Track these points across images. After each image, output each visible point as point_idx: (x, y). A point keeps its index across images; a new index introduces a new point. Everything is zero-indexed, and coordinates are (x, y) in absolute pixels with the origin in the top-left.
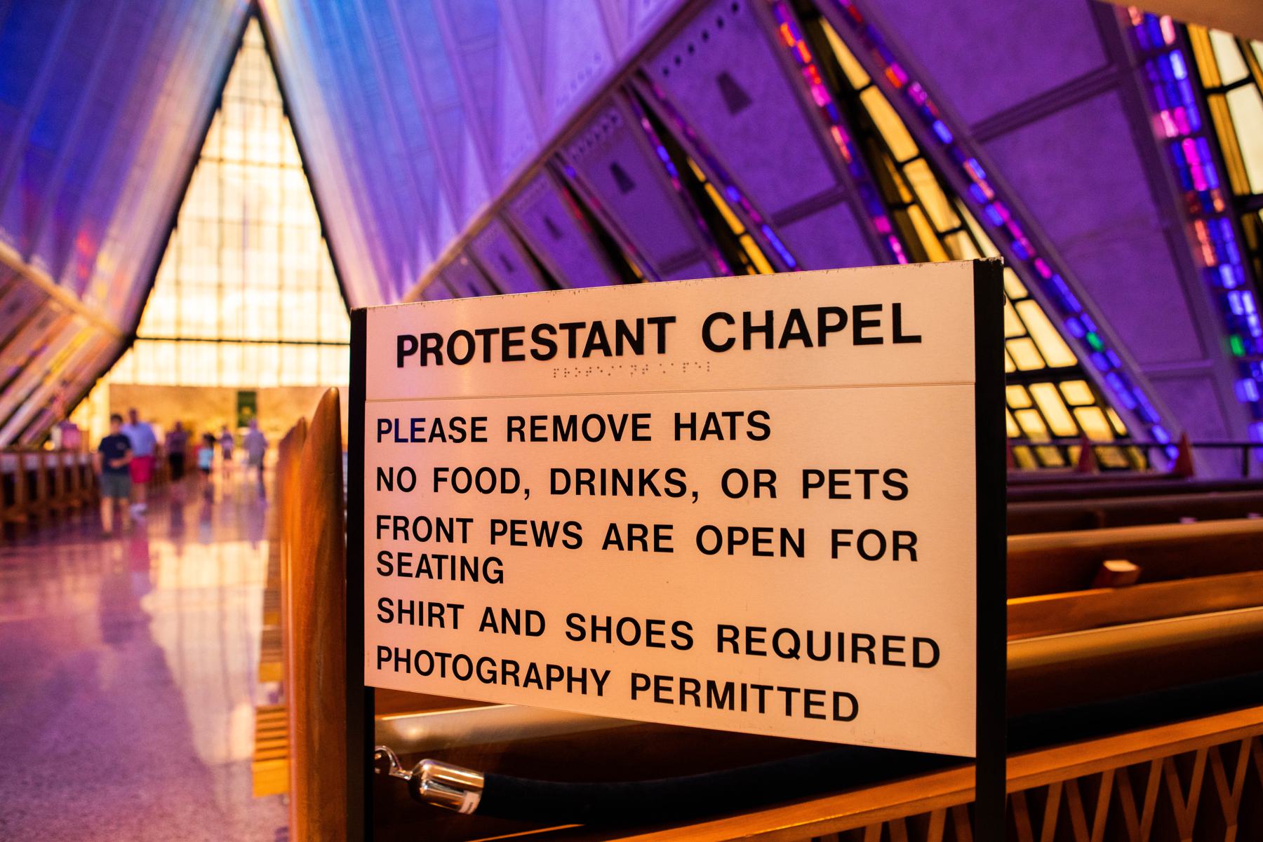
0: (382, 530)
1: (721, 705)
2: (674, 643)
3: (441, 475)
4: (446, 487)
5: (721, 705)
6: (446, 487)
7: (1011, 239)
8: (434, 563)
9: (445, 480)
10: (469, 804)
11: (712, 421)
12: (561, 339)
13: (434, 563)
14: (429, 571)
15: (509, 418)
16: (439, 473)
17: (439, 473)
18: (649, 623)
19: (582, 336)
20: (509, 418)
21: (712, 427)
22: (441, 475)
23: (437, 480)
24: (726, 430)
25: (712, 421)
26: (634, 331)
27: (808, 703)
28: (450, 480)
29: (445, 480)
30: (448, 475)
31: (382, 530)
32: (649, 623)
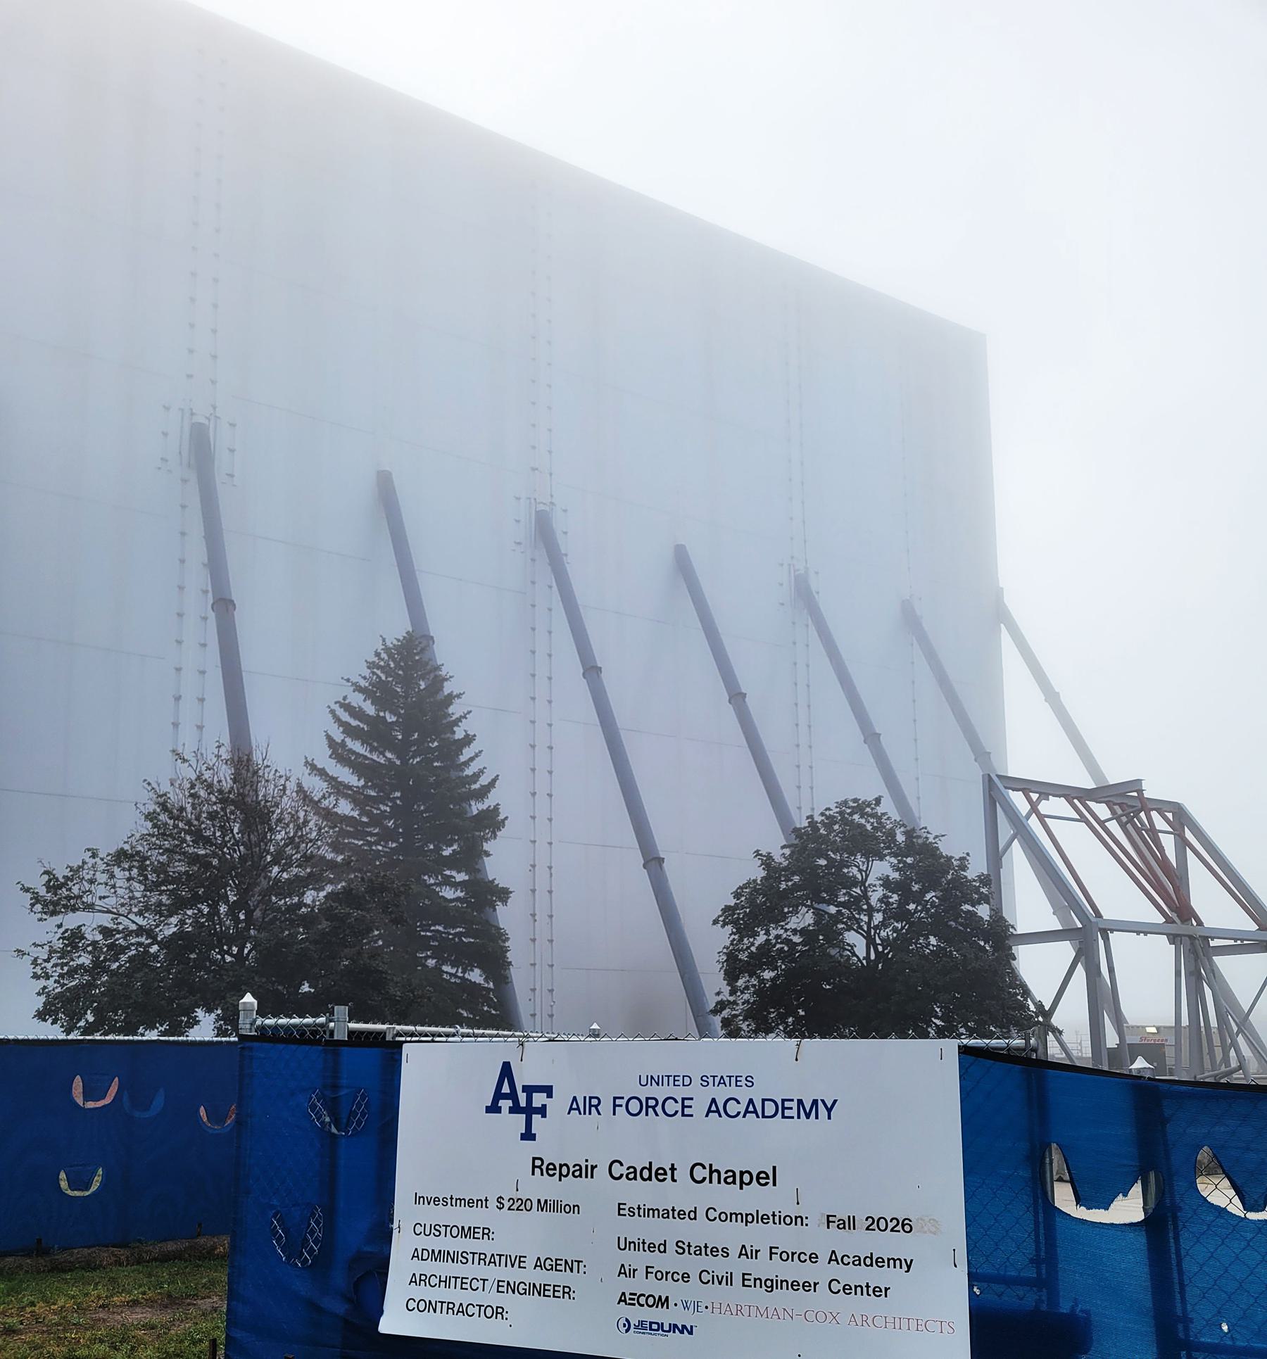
0: (617, 1108)
1: (808, 1116)
2: (746, 1085)
3: (618, 1102)
4: (621, 1111)
5: (808, 1116)
6: (621, 1111)
7: (74, 989)
8: (497, 1258)
9: (621, 1106)
10: (505, 816)
11: (808, 1111)
12: (711, 1080)
13: (497, 1258)
14: (495, 1262)
15: (762, 1099)
16: (685, 1101)
17: (685, 1101)
18: (783, 1101)
19: (717, 1080)
20: (762, 1099)
21: (722, 1081)
22: (618, 1102)
23: (615, 1106)
24: (728, 1084)
25: (808, 1111)
26: (689, 1329)
27: (737, 1081)
28: (624, 1106)
29: (621, 1106)
30: (623, 1102)
31: (617, 1108)
32: (783, 1101)
